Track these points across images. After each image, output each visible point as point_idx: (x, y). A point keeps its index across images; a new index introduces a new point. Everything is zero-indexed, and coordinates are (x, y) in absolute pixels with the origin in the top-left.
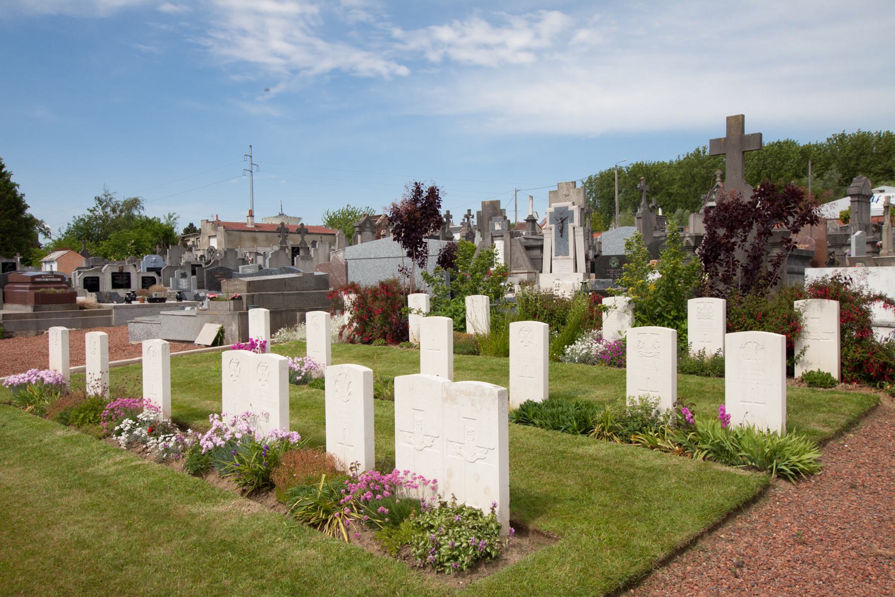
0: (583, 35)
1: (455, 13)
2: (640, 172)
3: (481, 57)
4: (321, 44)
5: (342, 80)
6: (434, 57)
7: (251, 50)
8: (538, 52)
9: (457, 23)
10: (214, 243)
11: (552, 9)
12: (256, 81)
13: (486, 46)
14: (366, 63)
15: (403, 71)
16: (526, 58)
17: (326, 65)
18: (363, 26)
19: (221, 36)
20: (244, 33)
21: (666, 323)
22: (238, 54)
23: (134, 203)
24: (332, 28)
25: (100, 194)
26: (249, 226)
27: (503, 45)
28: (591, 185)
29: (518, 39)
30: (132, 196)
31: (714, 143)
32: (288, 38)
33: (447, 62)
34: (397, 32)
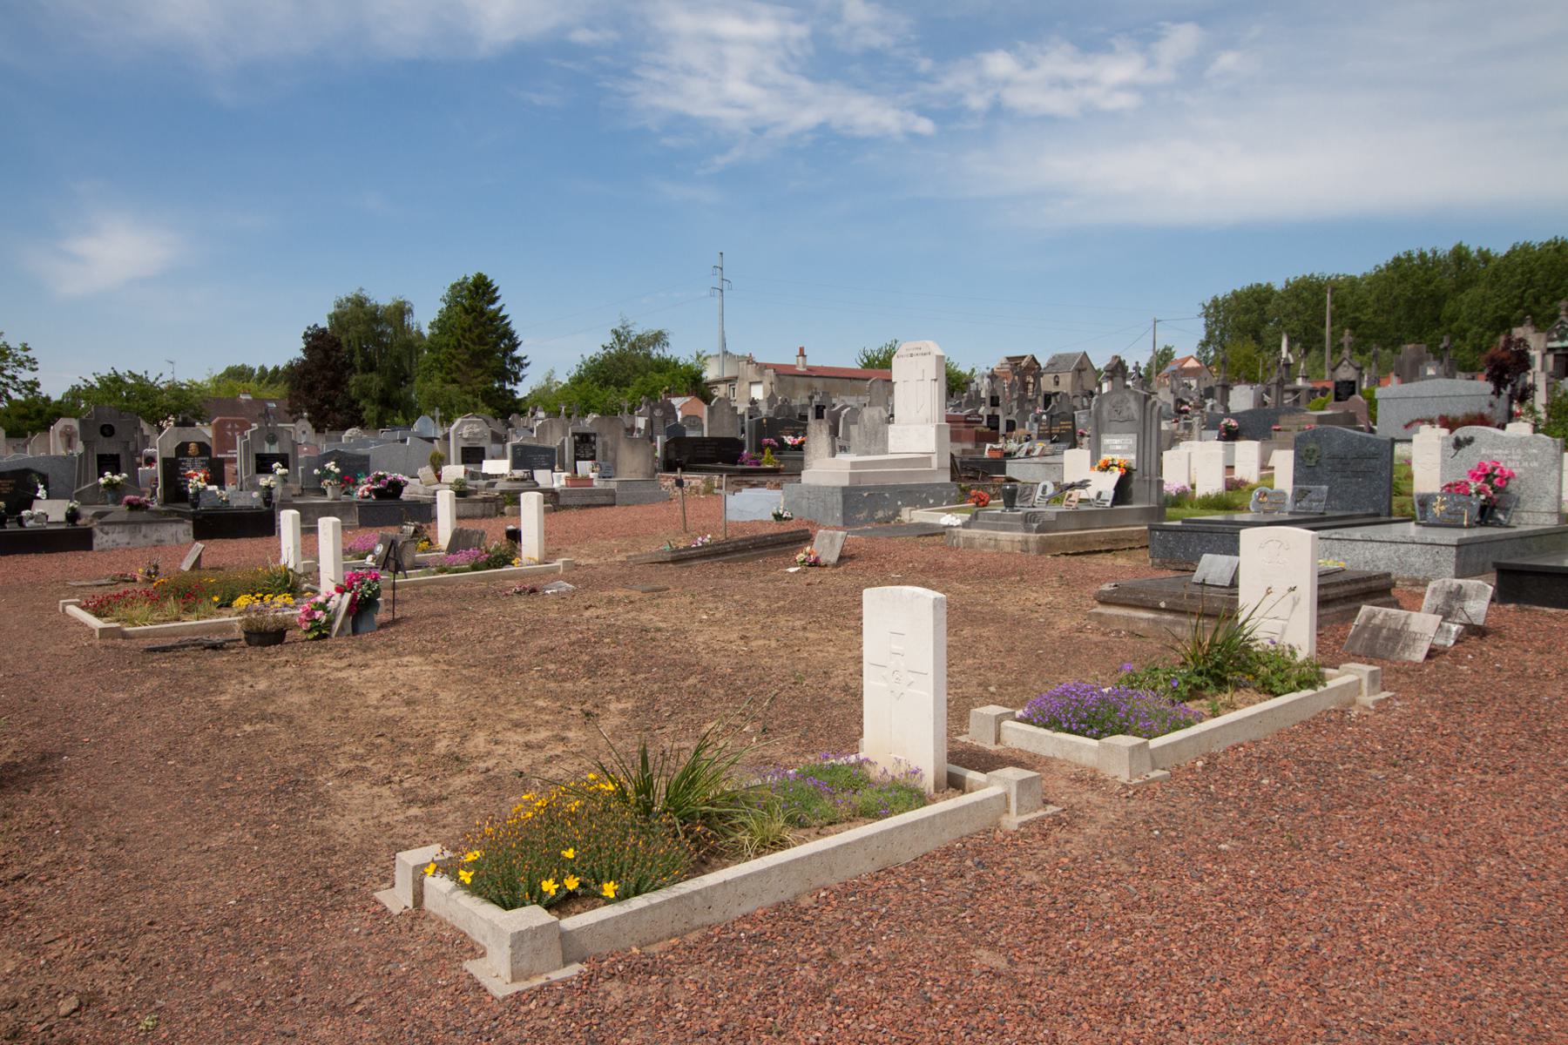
0: (1227, 60)
1: (1021, 31)
2: (1308, 294)
3: (1055, 103)
4: (805, 86)
5: (830, 143)
6: (977, 102)
7: (698, 99)
8: (1145, 91)
9: (1023, 45)
10: (758, 393)
11: (1179, 19)
12: (689, 147)
13: (1063, 84)
14: (869, 113)
15: (925, 126)
16: (1124, 101)
17: (809, 117)
18: (873, 57)
19: (657, 75)
20: (689, 71)
21: (379, 909)
22: (674, 103)
23: (658, 338)
24: (828, 61)
25: (617, 326)
26: (800, 369)
27: (1084, 82)
28: (1216, 307)
29: (1119, 69)
30: (656, 329)
31: (1485, 257)
32: (753, 79)
33: (997, 111)
34: (925, 65)
